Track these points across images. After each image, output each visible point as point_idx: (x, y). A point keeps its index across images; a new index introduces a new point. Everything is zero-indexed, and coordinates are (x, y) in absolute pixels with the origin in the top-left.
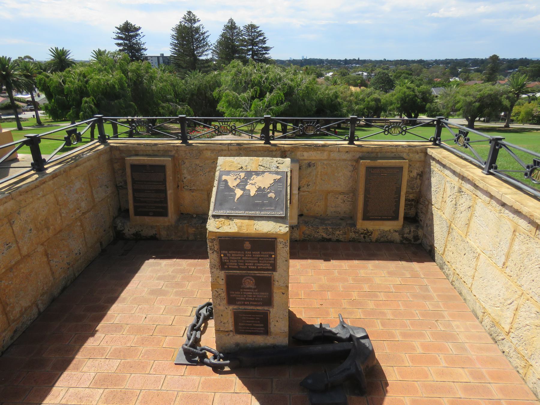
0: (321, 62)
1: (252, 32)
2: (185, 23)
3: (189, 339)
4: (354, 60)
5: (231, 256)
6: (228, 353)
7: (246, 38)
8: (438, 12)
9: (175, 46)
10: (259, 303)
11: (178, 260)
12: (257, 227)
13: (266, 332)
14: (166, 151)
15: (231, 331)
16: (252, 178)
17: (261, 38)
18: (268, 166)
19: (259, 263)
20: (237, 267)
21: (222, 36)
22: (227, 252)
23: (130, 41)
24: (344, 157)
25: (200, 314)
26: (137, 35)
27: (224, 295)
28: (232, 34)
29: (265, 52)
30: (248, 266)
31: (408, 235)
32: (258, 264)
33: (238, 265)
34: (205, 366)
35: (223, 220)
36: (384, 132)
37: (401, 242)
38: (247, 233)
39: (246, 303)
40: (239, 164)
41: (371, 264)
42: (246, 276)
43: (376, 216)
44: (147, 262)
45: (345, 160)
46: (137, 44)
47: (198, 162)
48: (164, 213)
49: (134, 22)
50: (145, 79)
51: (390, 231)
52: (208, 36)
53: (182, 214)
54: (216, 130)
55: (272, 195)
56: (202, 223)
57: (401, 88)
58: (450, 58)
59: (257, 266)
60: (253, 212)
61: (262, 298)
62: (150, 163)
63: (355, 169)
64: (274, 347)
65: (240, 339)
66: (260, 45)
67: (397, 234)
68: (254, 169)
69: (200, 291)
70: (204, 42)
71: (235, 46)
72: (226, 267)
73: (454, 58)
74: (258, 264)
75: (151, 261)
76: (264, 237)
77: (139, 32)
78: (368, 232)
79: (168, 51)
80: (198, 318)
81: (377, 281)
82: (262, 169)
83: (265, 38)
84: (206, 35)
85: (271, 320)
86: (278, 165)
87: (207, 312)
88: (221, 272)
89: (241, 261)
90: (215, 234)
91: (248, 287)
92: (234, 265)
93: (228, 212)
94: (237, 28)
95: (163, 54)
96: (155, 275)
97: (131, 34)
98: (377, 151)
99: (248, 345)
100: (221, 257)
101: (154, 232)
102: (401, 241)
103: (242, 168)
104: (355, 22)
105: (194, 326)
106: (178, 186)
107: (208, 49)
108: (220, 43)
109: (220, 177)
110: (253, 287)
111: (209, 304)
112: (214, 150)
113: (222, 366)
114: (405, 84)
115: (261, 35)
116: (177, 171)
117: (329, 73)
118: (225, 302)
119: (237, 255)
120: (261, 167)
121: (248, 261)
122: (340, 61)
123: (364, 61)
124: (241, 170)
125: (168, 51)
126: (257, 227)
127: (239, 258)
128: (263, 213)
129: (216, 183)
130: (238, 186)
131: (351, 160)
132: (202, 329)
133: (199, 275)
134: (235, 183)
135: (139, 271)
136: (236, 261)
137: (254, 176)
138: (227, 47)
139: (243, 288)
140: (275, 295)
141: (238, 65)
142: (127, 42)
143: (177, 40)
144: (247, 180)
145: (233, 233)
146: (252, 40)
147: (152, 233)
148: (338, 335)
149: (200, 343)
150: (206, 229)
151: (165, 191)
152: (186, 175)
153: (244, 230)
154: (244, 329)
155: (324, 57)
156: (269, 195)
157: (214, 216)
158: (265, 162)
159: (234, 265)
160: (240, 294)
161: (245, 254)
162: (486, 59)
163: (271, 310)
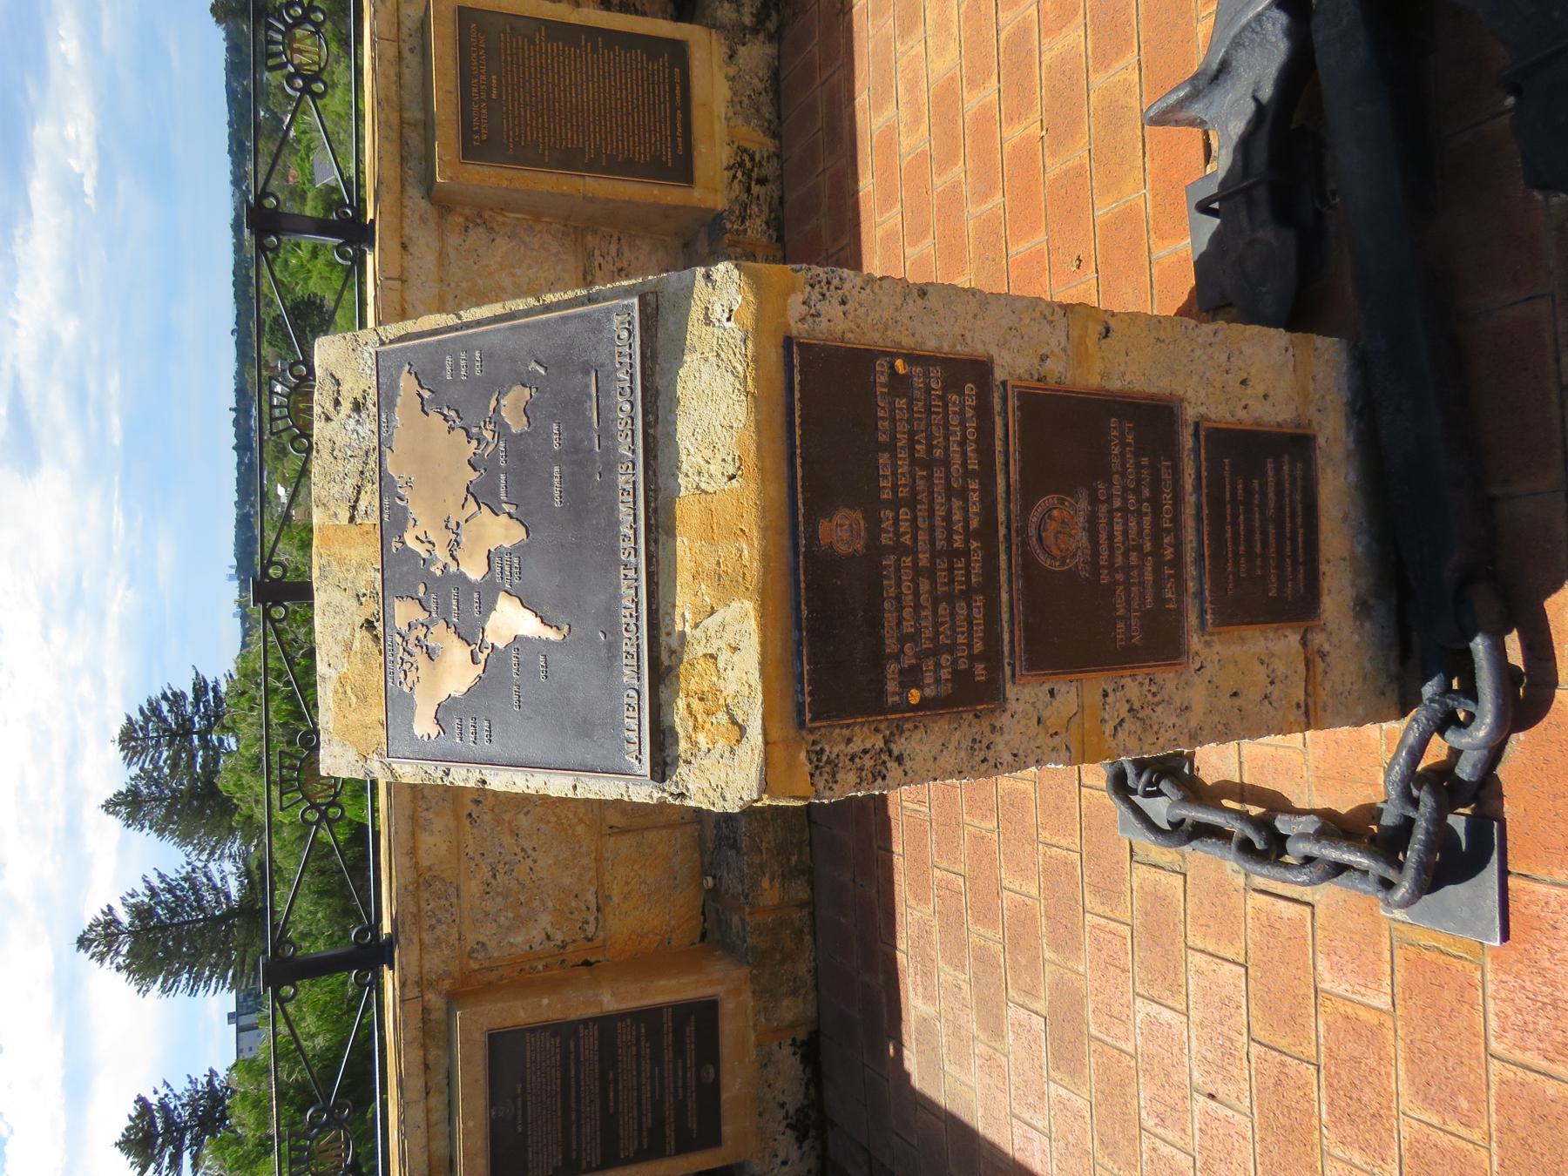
0: (243, 523)
1: (146, 737)
2: (117, 953)
3: (1339, 869)
4: (236, 422)
5: (914, 637)
6: (1404, 656)
7: (165, 754)
8: (82, 175)
9: (198, 978)
10: (1166, 476)
11: (902, 944)
12: (715, 469)
13: (1296, 445)
14: (430, 1034)
15: (1304, 642)
16: (420, 549)
17: (165, 707)
18: (354, 466)
19: (946, 463)
20: (979, 601)
21: (161, 832)
22: (892, 668)
23: (186, 1128)
24: (430, 260)
25: (1177, 825)
26: (163, 1106)
27: (1133, 687)
28: (155, 799)
29: (211, 694)
30: (968, 535)
31: (746, 9)
32: (956, 467)
33: (967, 596)
34: (1501, 771)
35: (681, 703)
36: (316, 96)
37: (775, 37)
38: (764, 530)
39: (1168, 554)
40: (348, 647)
41: (873, 118)
42: (1025, 543)
43: (674, 129)
44: (916, 1082)
45: (442, 255)
46: (193, 1103)
47: (473, 888)
48: (706, 1012)
49: (118, 1118)
50: (289, 1075)
51: (729, 79)
52: (160, 875)
53: (704, 936)
54: (323, 815)
55: (512, 406)
56: (738, 850)
57: (315, 274)
58: (227, 142)
59: (967, 474)
60: (624, 511)
61: (1137, 454)
62: (481, 1103)
63: (481, 214)
64: (1366, 409)
65: (1339, 588)
66: (189, 709)
67: (742, 50)
68: (369, 551)
69: (1045, 835)
70: (182, 889)
71: (192, 788)
72: (979, 668)
73: (226, 130)
74: (956, 467)
75: (911, 1062)
76: (779, 419)
77: (153, 1100)
78: (741, 164)
79: (219, 1001)
80: (1203, 831)
81: (944, 62)
82: (369, 499)
83: (165, 697)
84: (156, 882)
85: (1241, 414)
86: (346, 406)
87: (1159, 793)
88: (1012, 705)
89: (942, 576)
90: (778, 752)
91: (1082, 538)
92: (970, 620)
93: (628, 676)
94: (136, 786)
95: (231, 1016)
96: (980, 1048)
97: (160, 1126)
98: (394, 118)
99: (1359, 549)
100: (924, 704)
101: (788, 1049)
102: (770, 38)
103: (369, 625)
104: (115, 423)
105: (1246, 847)
106: (587, 963)
107: (205, 875)
108: (185, 838)
109: (423, 753)
110: (1083, 505)
111: (1120, 785)
112: (414, 818)
113: (1507, 676)
114: (302, 266)
115: (155, 709)
116: (523, 976)
117: (278, 497)
118: (1167, 678)
119: (908, 600)
120: (362, 505)
121: (940, 534)
122: (239, 464)
123: (241, 392)
124: (379, 626)
125: (219, 1001)
126: (715, 469)
127: (924, 585)
128: (630, 446)
129: (463, 776)
130: (469, 634)
131: (442, 235)
132: (1255, 811)
133: (965, 846)
134: (457, 653)
135: (965, 1117)
136: (943, 608)
137: (412, 543)
138: (200, 812)
139: (1095, 566)
140: (1116, 385)
141: (233, 770)
142: (188, 1136)
143: (178, 974)
144: (432, 583)
145: (763, 628)
146: (173, 735)
147: (788, 1062)
148: (1266, 93)
149: (1343, 810)
150: (749, 812)
151: (607, 1022)
152: (537, 935)
153: (746, 552)
154: (1295, 564)
155: (230, 515)
156: (517, 424)
157: (662, 767)
158: (335, 489)
159: (970, 620)
160: (1127, 584)
161: (899, 549)
162: (228, 38)
163: (1191, 413)
